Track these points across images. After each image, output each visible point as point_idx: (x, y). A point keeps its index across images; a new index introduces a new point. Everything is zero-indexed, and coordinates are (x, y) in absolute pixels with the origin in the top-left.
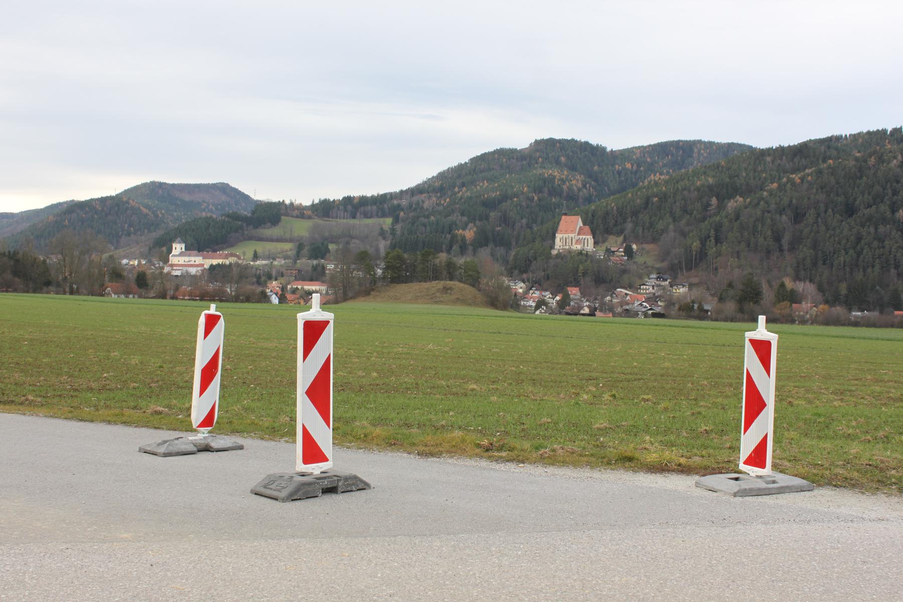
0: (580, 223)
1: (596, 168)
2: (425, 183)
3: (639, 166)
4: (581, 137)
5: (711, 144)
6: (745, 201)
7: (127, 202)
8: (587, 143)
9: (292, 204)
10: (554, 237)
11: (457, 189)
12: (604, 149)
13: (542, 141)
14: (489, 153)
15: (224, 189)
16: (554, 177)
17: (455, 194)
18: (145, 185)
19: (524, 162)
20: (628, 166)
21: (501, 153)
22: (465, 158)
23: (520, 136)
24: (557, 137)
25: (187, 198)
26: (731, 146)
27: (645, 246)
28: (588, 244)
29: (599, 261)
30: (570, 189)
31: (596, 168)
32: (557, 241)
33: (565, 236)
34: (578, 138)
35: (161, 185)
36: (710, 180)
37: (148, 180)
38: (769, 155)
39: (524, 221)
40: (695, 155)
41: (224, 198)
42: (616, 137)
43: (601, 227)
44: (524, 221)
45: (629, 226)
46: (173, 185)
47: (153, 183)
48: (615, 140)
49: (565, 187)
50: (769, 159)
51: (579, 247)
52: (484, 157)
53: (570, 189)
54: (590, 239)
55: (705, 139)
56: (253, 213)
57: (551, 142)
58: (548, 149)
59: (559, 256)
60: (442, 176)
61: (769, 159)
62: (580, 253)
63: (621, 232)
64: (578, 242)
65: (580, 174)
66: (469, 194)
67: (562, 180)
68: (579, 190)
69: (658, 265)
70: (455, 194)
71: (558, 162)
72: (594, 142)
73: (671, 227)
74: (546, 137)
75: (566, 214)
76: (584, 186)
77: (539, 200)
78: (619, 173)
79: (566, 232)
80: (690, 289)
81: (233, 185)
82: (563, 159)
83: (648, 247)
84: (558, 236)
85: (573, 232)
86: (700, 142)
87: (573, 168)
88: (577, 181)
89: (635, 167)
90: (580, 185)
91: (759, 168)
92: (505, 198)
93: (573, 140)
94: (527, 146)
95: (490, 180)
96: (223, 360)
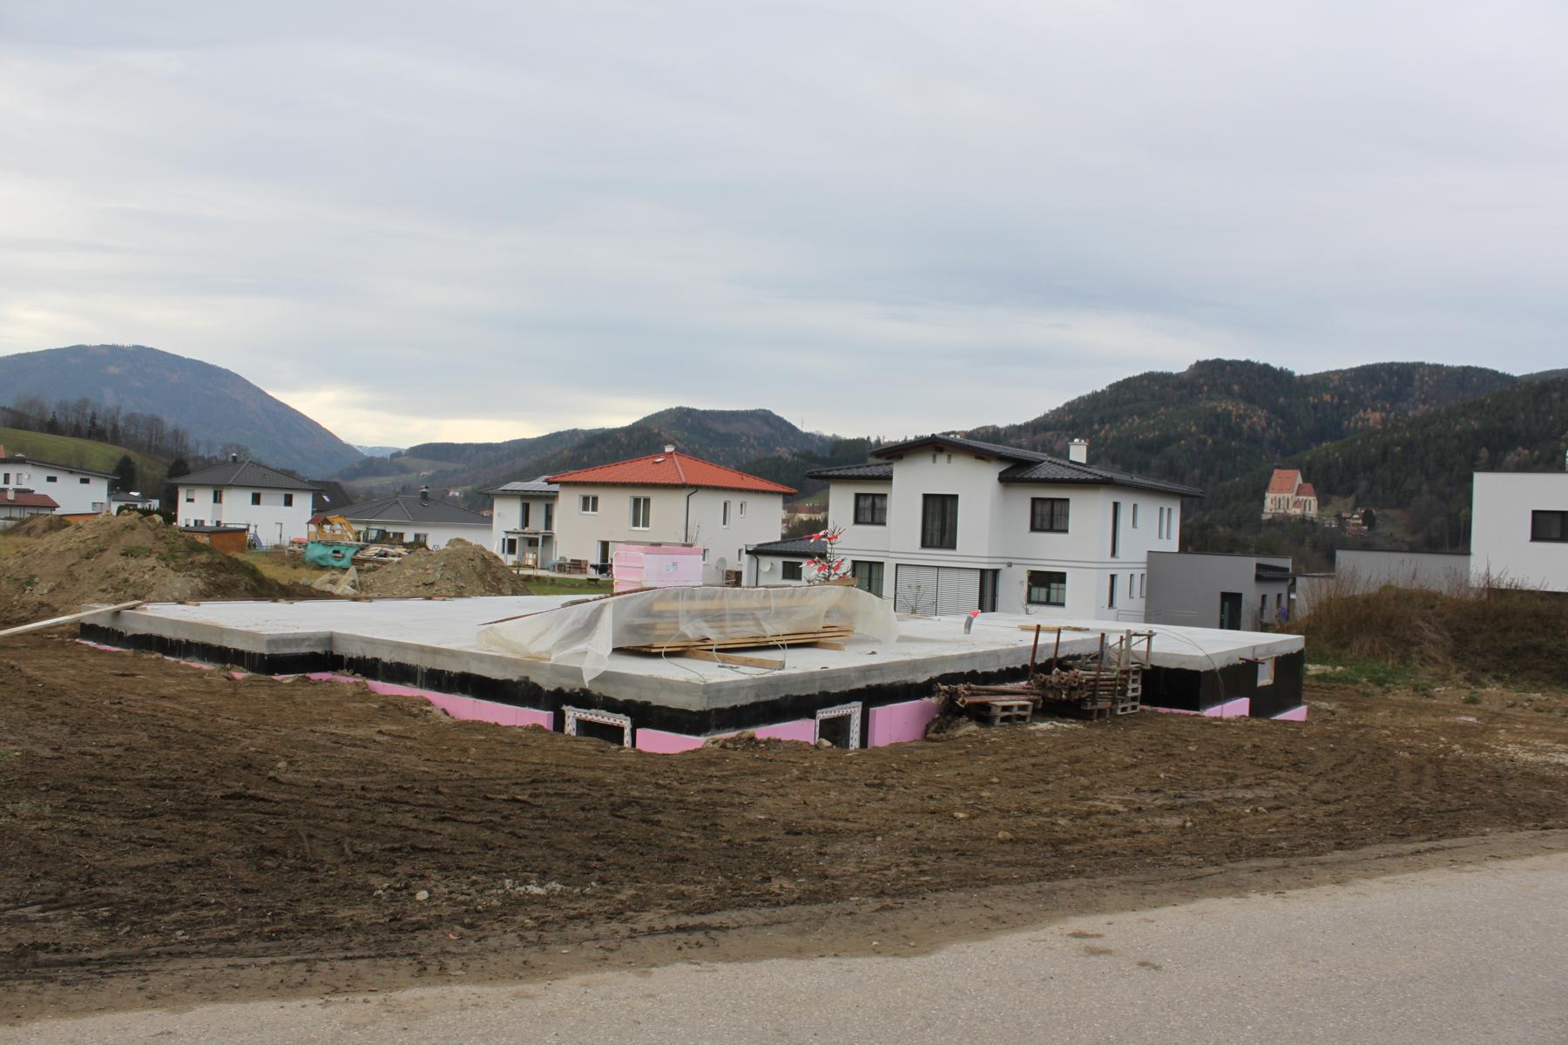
0: (1299, 480)
1: (1282, 400)
2: (1046, 416)
3: (1342, 398)
4: (1259, 358)
5: (1437, 368)
6: (1531, 454)
7: (659, 435)
8: (1266, 366)
9: (878, 441)
10: (1262, 500)
11: (1096, 427)
12: (1290, 374)
13: (1206, 363)
14: (1135, 379)
15: (766, 417)
16: (1230, 413)
17: (1096, 432)
18: (669, 412)
19: (1184, 391)
20: (1327, 397)
21: (1151, 378)
22: (1101, 385)
23: (1176, 354)
24: (1227, 358)
25: (722, 429)
26: (1467, 372)
27: (1387, 511)
28: (1310, 506)
29: (1326, 531)
30: (1252, 427)
31: (1282, 400)
32: (1268, 502)
33: (1279, 495)
34: (1254, 359)
35: (690, 412)
36: (1475, 424)
37: (673, 404)
38: (1555, 390)
39: (1197, 472)
40: (1417, 383)
41: (766, 429)
42: (1306, 357)
43: (1324, 482)
44: (1197, 472)
45: (1363, 485)
46: (704, 412)
47: (680, 409)
48: (1304, 361)
49: (1245, 426)
50: (1556, 395)
51: (1298, 511)
52: (1127, 384)
53: (1252, 427)
54: (1313, 501)
55: (1430, 361)
56: (833, 453)
57: (1218, 365)
58: (1213, 374)
59: (1271, 522)
60: (1071, 407)
61: (1556, 395)
62: (1303, 519)
63: (1351, 491)
64: (1296, 504)
65: (1262, 408)
66: (1115, 433)
67: (1240, 416)
68: (1264, 429)
69: (1408, 539)
70: (1096, 432)
71: (1229, 393)
72: (1276, 364)
73: (1425, 487)
74: (1211, 358)
75: (1279, 467)
76: (1269, 425)
77: (1214, 443)
78: (1315, 407)
79: (1280, 491)
80: (320, 515)
81: (777, 412)
82: (1236, 387)
83: (1392, 513)
84: (1269, 496)
85: (1289, 491)
86: (1421, 365)
87: (1250, 400)
88: (1258, 418)
89: (1336, 400)
90: (1263, 423)
91: (1543, 408)
92: (1166, 440)
93: (1248, 362)
94: (1184, 368)
95: (1143, 414)
96: (34, 633)
